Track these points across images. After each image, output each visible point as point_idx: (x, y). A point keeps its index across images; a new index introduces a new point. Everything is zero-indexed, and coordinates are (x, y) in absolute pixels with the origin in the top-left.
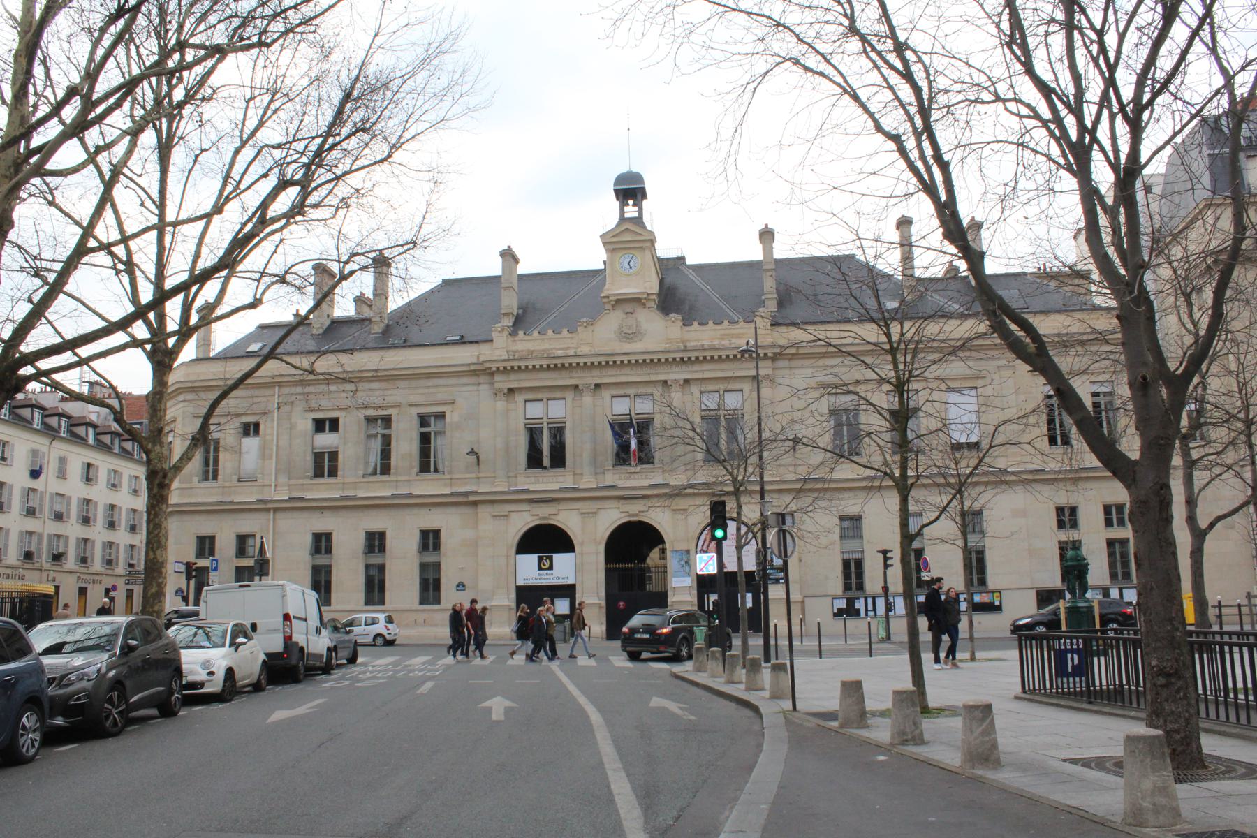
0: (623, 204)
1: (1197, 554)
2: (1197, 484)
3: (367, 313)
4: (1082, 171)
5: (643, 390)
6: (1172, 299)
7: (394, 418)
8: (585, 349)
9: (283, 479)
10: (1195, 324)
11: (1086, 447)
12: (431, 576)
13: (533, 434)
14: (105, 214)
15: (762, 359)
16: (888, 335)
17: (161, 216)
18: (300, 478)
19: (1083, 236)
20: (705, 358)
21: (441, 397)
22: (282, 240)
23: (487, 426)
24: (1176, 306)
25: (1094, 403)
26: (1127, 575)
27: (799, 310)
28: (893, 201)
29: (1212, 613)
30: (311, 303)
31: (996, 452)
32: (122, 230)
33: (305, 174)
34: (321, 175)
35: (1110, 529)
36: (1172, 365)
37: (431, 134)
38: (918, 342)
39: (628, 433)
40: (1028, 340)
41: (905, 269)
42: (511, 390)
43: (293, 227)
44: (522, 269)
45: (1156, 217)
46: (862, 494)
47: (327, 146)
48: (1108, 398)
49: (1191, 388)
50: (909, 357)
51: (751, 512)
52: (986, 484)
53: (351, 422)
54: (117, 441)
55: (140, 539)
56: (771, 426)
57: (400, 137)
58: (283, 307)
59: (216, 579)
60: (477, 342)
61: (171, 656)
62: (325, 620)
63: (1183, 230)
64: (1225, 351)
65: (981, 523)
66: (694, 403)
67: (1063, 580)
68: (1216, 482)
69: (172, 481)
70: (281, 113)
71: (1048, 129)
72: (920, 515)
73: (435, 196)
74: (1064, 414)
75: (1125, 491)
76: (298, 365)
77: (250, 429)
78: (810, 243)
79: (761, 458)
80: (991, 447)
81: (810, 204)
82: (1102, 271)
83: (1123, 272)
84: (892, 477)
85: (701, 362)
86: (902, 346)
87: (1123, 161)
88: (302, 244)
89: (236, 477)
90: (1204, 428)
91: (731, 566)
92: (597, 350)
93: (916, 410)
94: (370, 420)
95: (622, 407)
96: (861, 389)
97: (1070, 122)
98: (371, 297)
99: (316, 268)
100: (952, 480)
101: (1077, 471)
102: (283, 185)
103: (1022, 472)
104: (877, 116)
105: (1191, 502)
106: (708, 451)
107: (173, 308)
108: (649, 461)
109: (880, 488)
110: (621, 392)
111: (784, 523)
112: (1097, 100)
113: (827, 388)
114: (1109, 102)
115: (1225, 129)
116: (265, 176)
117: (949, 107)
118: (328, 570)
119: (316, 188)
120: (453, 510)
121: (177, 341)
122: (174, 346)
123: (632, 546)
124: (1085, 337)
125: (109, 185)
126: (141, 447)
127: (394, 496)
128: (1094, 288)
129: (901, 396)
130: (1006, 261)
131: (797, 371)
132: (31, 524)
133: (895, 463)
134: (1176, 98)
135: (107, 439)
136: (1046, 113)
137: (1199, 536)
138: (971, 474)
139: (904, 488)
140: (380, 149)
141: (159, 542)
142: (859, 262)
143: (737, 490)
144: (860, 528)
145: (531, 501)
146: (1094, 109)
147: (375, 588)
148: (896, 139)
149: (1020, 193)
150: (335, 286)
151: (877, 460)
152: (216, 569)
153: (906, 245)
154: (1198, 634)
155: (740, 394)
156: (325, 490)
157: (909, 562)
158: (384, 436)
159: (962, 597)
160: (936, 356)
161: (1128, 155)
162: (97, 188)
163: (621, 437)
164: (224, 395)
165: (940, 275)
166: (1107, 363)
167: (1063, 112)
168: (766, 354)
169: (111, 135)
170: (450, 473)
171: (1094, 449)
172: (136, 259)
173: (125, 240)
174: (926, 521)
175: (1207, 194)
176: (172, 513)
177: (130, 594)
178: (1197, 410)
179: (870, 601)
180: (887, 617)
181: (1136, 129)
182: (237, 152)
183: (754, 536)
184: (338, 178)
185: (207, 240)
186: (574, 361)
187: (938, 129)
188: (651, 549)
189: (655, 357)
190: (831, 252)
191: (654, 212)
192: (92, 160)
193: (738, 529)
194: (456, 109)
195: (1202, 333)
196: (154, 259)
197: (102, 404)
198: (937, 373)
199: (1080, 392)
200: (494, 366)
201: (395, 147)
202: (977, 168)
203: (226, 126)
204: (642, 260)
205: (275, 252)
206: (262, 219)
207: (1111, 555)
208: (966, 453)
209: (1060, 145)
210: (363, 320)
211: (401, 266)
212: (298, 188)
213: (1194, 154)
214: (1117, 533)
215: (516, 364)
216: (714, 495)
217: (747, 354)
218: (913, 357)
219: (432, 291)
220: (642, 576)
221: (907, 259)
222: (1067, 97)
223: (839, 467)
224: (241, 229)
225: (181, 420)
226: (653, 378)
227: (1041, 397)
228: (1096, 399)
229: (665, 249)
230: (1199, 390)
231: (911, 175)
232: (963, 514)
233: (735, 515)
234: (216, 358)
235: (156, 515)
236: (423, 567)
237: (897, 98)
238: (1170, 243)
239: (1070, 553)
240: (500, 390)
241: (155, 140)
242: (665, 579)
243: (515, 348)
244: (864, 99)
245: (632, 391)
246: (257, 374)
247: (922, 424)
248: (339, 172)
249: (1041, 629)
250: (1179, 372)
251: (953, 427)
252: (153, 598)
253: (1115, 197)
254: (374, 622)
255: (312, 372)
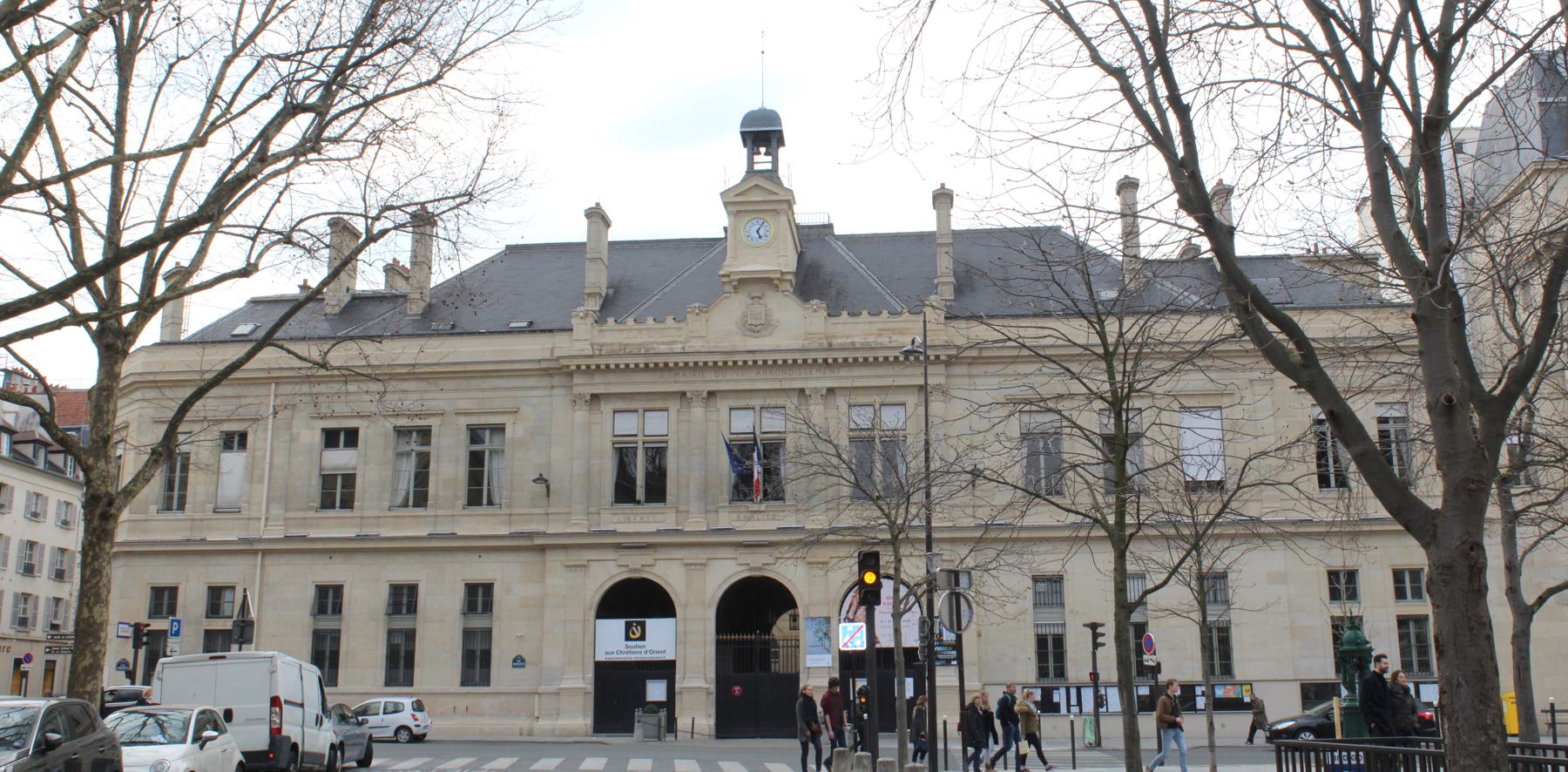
0: (753, 152)
1: (1521, 639)
2: (1521, 545)
3: (401, 286)
4: (1369, 122)
5: (771, 401)
6: (1489, 294)
7: (434, 430)
8: (696, 345)
9: (277, 511)
10: (1519, 329)
11: (1369, 491)
12: (478, 647)
13: (624, 456)
14: (38, 140)
15: (933, 363)
16: (1102, 335)
17: (119, 145)
18: (298, 510)
19: (1368, 209)
20: (856, 359)
21: (500, 402)
22: (287, 186)
23: (563, 443)
24: (1493, 304)
25: (1380, 432)
26: (1425, 666)
27: (984, 299)
28: (1113, 156)
29: (1542, 720)
30: (324, 272)
31: (1245, 494)
32: (61, 162)
33: (323, 98)
34: (344, 99)
35: (1402, 603)
36: (1487, 383)
37: (496, 50)
38: (1141, 346)
39: (751, 458)
40: (1291, 346)
41: (1126, 247)
42: (595, 397)
43: (303, 168)
44: (615, 234)
45: (1468, 185)
46: (1064, 547)
47: (353, 60)
48: (1400, 426)
49: (1513, 414)
50: (1129, 365)
51: (914, 569)
52: (1233, 537)
53: (375, 434)
54: (42, 453)
55: (70, 590)
56: (943, 453)
57: (455, 52)
58: (285, 275)
59: (176, 648)
60: (551, 331)
61: (108, 755)
62: (330, 705)
63: (1504, 202)
64: (1559, 366)
65: (1225, 590)
66: (839, 421)
67: (1338, 671)
68: (1547, 542)
69: (120, 510)
70: (290, 12)
71: (1324, 64)
72: (1141, 576)
73: (499, 133)
74: (1340, 445)
75: (1422, 551)
76: (305, 355)
77: (235, 441)
78: (999, 210)
79: (928, 495)
80: (1239, 488)
81: (1000, 158)
82: (1394, 258)
83: (1421, 257)
84: (1105, 525)
85: (850, 365)
86: (1121, 350)
87: (1424, 110)
88: (317, 191)
89: (211, 506)
90: (1531, 469)
91: (886, 640)
92: (712, 346)
93: (1139, 436)
94: (401, 432)
95: (743, 423)
96: (1063, 406)
97: (1354, 56)
98: (408, 266)
99: (332, 224)
100: (1186, 532)
101: (1355, 523)
102: (292, 109)
103: (1280, 522)
104: (1094, 43)
105: (1513, 569)
106: (857, 485)
107: (132, 273)
108: (779, 496)
109: (1087, 539)
110: (742, 403)
111: (957, 584)
112: (1391, 27)
113: (1018, 404)
114: (1408, 31)
115: (1562, 70)
116: (267, 96)
117: (1191, 33)
118: (335, 636)
119: (336, 117)
120: (511, 557)
121: (136, 317)
122: (131, 324)
123: (753, 609)
124: (1369, 343)
125: (45, 103)
126: (78, 460)
127: (431, 536)
128: (1382, 278)
129: (1118, 416)
130: (1263, 240)
131: (978, 381)
132: (28, 585)
133: (1109, 506)
134: (1497, 27)
135: (28, 450)
136: (1322, 44)
137: (1524, 614)
138: (1212, 523)
139: (1120, 541)
140: (425, 67)
141: (98, 595)
142: (1065, 236)
143: (895, 538)
144: (1062, 597)
145: (619, 546)
146: (1387, 39)
147: (400, 662)
148: (1119, 73)
149: (1284, 150)
150: (359, 250)
151: (1084, 502)
152: (177, 634)
153: (1129, 215)
154: (1523, 748)
155: (901, 409)
156: (335, 526)
157: (1127, 641)
158: (419, 454)
159: (1199, 690)
160: (1166, 364)
161: (1432, 103)
162: (28, 106)
163: (741, 463)
164: (199, 394)
165: (1174, 257)
166: (1399, 378)
167: (1345, 42)
168: (937, 357)
169: (50, 31)
170: (510, 506)
171: (1379, 493)
172: (81, 203)
173: (66, 177)
174: (1150, 585)
175: (1537, 156)
176: (117, 555)
177: (50, 668)
178: (1521, 445)
179: (1073, 692)
180: (1097, 715)
181: (1443, 68)
182: (228, 62)
183: (918, 601)
184: (367, 104)
185: (182, 181)
186: (681, 360)
187: (1177, 64)
188: (779, 615)
189: (790, 357)
190: (1028, 222)
191: (792, 164)
192: (22, 64)
193: (896, 591)
194: (531, 17)
195: (1528, 341)
196: (107, 204)
197: (23, 401)
198: (1168, 387)
199: (1360, 416)
200: (573, 364)
201: (447, 65)
202: (1227, 115)
203: (213, 27)
204: (777, 228)
205: (278, 201)
206: (259, 160)
207: (1403, 637)
208: (1206, 495)
209: (1340, 86)
210: (396, 296)
211: (451, 226)
212: (311, 116)
213: (1521, 102)
214: (1412, 608)
215: (602, 362)
216: (864, 543)
217: (911, 355)
218: (1136, 365)
219: (492, 261)
220: (766, 652)
221: (1130, 234)
222: (1351, 23)
223: (1033, 510)
224: (231, 168)
225: (137, 425)
226: (786, 385)
227: (1308, 422)
228: (1384, 427)
229: (807, 213)
230: (1525, 417)
231: (1138, 122)
232: (1201, 578)
233: (892, 572)
234: (189, 343)
235: (96, 557)
236: (468, 634)
237: (1122, 19)
238: (1486, 219)
239: (1347, 634)
240: (581, 396)
241: (114, 44)
242: (797, 658)
243: (602, 341)
244: (1077, 20)
245: (757, 402)
246: (246, 366)
247: (1146, 454)
248: (369, 96)
249: (1308, 737)
250: (1496, 393)
251: (1188, 459)
252: (84, 673)
253: (1413, 157)
254: (397, 709)
255: (324, 366)
